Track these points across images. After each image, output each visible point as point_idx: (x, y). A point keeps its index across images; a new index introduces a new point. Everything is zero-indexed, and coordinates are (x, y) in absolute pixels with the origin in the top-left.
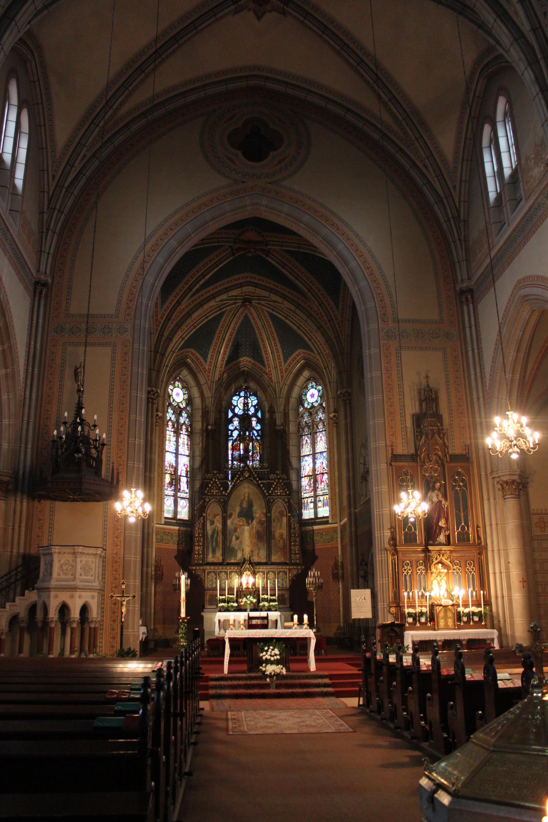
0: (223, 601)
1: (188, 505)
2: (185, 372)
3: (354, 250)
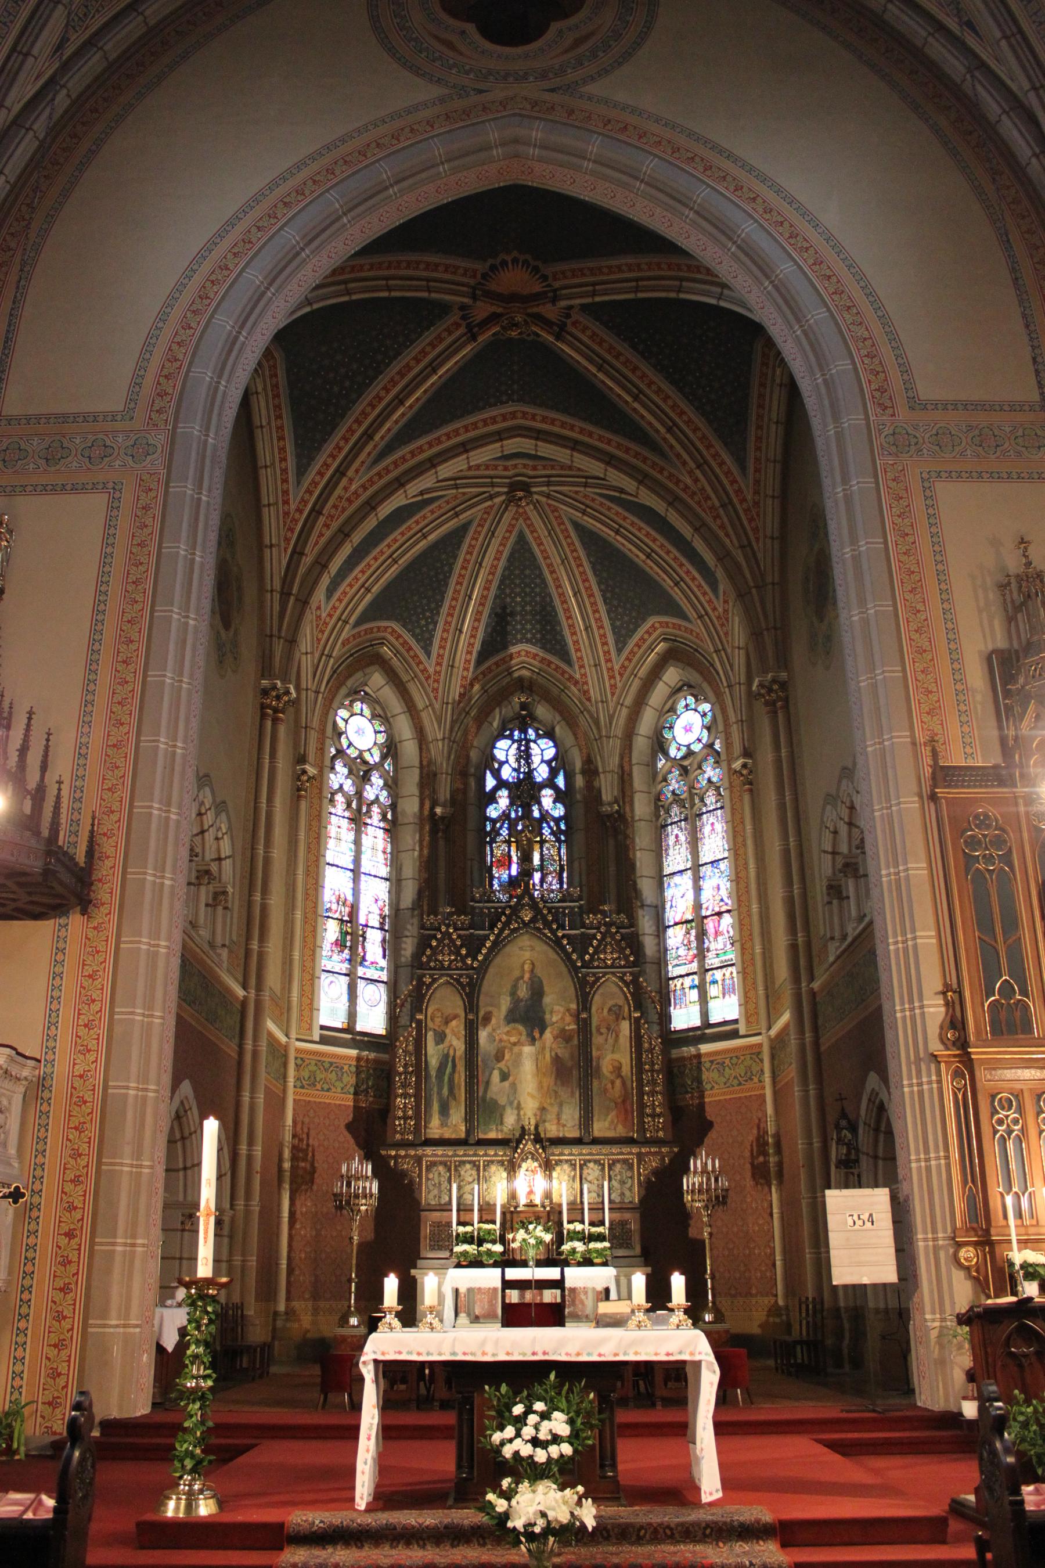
0: (468, 1239)
1: (384, 997)
2: (377, 679)
3: (787, 235)
